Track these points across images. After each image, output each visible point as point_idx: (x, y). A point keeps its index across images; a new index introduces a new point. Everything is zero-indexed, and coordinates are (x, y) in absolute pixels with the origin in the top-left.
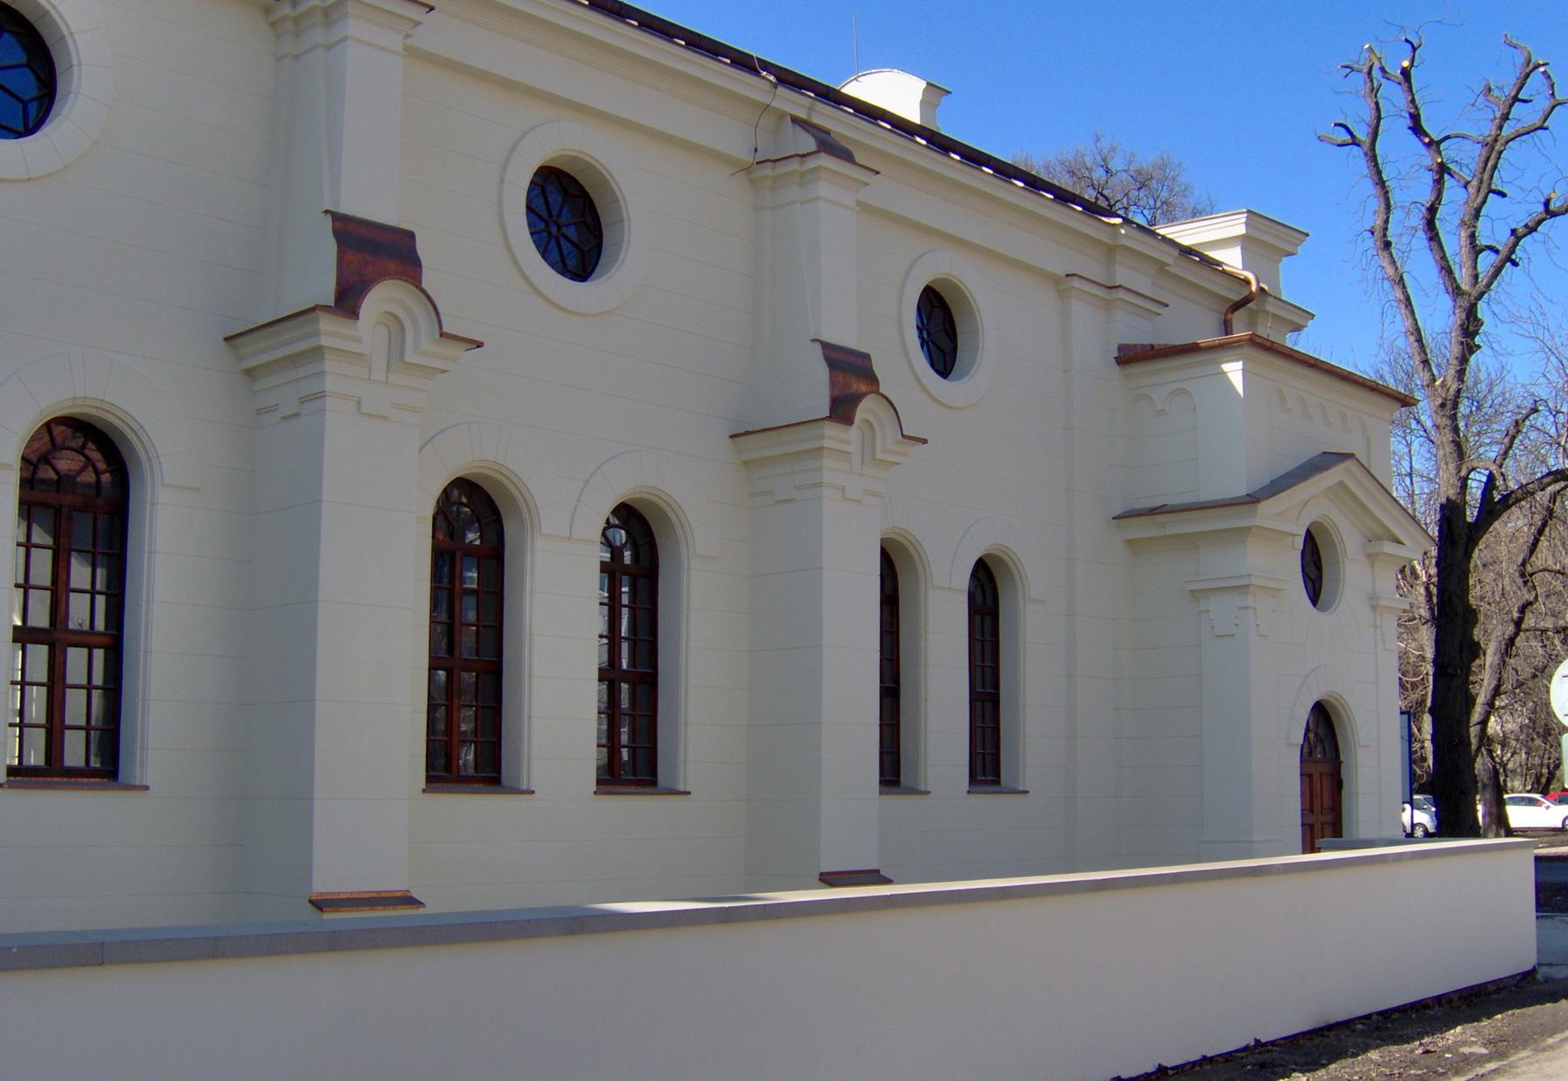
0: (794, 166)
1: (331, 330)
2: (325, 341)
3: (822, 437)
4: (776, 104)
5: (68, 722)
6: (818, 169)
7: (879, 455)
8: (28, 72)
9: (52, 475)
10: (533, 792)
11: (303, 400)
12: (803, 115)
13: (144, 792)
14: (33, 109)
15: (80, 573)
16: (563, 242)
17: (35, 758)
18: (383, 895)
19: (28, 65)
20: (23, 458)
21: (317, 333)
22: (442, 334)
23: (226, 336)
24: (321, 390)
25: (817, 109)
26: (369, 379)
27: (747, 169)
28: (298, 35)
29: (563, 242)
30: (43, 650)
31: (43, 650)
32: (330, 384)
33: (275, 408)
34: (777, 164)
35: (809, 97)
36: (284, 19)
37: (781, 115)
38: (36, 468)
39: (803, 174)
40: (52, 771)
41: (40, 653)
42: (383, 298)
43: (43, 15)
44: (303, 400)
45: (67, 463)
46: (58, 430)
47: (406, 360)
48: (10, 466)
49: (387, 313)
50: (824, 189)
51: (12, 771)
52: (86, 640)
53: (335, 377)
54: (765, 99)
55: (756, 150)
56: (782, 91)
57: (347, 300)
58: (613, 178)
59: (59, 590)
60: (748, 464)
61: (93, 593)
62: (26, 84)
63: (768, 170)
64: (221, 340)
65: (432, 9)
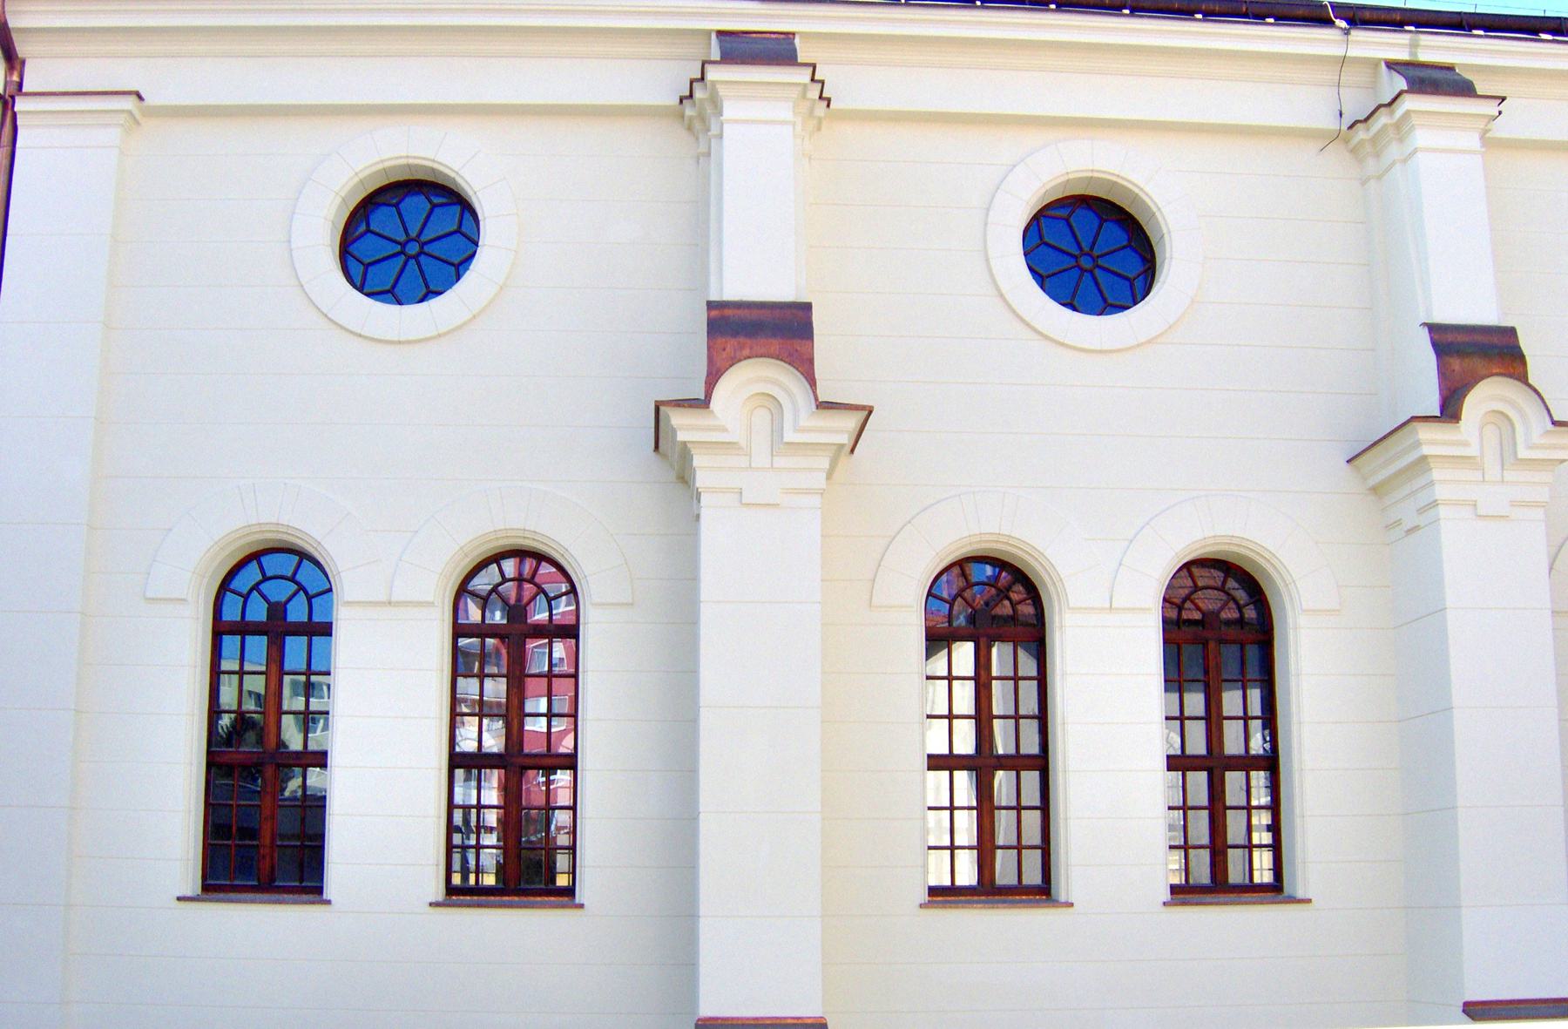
0: (1382, 119)
1: (1433, 439)
2: (1426, 450)
3: (1418, 444)
4: (1353, 52)
5: (1230, 842)
6: (1408, 113)
7: (1523, 453)
8: (402, 206)
9: (1197, 616)
10: (1072, 905)
11: (1421, 511)
12: (1404, 56)
13: (1307, 905)
14: (1138, 284)
15: (1231, 701)
16: (429, 234)
17: (1202, 874)
18: (789, 1021)
19: (1129, 246)
20: (1165, 600)
21: (1418, 444)
22: (1554, 423)
23: (1347, 459)
24: (1431, 500)
25: (1422, 43)
26: (1484, 481)
27: (1337, 136)
28: (1377, 155)
29: (429, 234)
30: (1202, 776)
31: (1202, 776)
32: (1440, 492)
33: (1398, 523)
34: (1370, 121)
35: (1410, 32)
36: (1362, 142)
37: (1374, 63)
38: (1180, 608)
39: (1398, 126)
40: (987, 890)
41: (1199, 780)
42: (1484, 398)
43: (1135, 198)
44: (1421, 511)
45: (1209, 601)
46: (1204, 577)
47: (1520, 456)
48: (1149, 609)
49: (1486, 413)
50: (1422, 137)
51: (1175, 889)
52: (1016, 763)
53: (1445, 484)
54: (1338, 51)
55: (1341, 115)
56: (1358, 35)
57: (1450, 410)
58: (1142, 189)
59: (1213, 719)
60: (1374, 490)
61: (1246, 718)
62: (1132, 266)
63: (1361, 134)
64: (1343, 463)
65: (1503, 99)
